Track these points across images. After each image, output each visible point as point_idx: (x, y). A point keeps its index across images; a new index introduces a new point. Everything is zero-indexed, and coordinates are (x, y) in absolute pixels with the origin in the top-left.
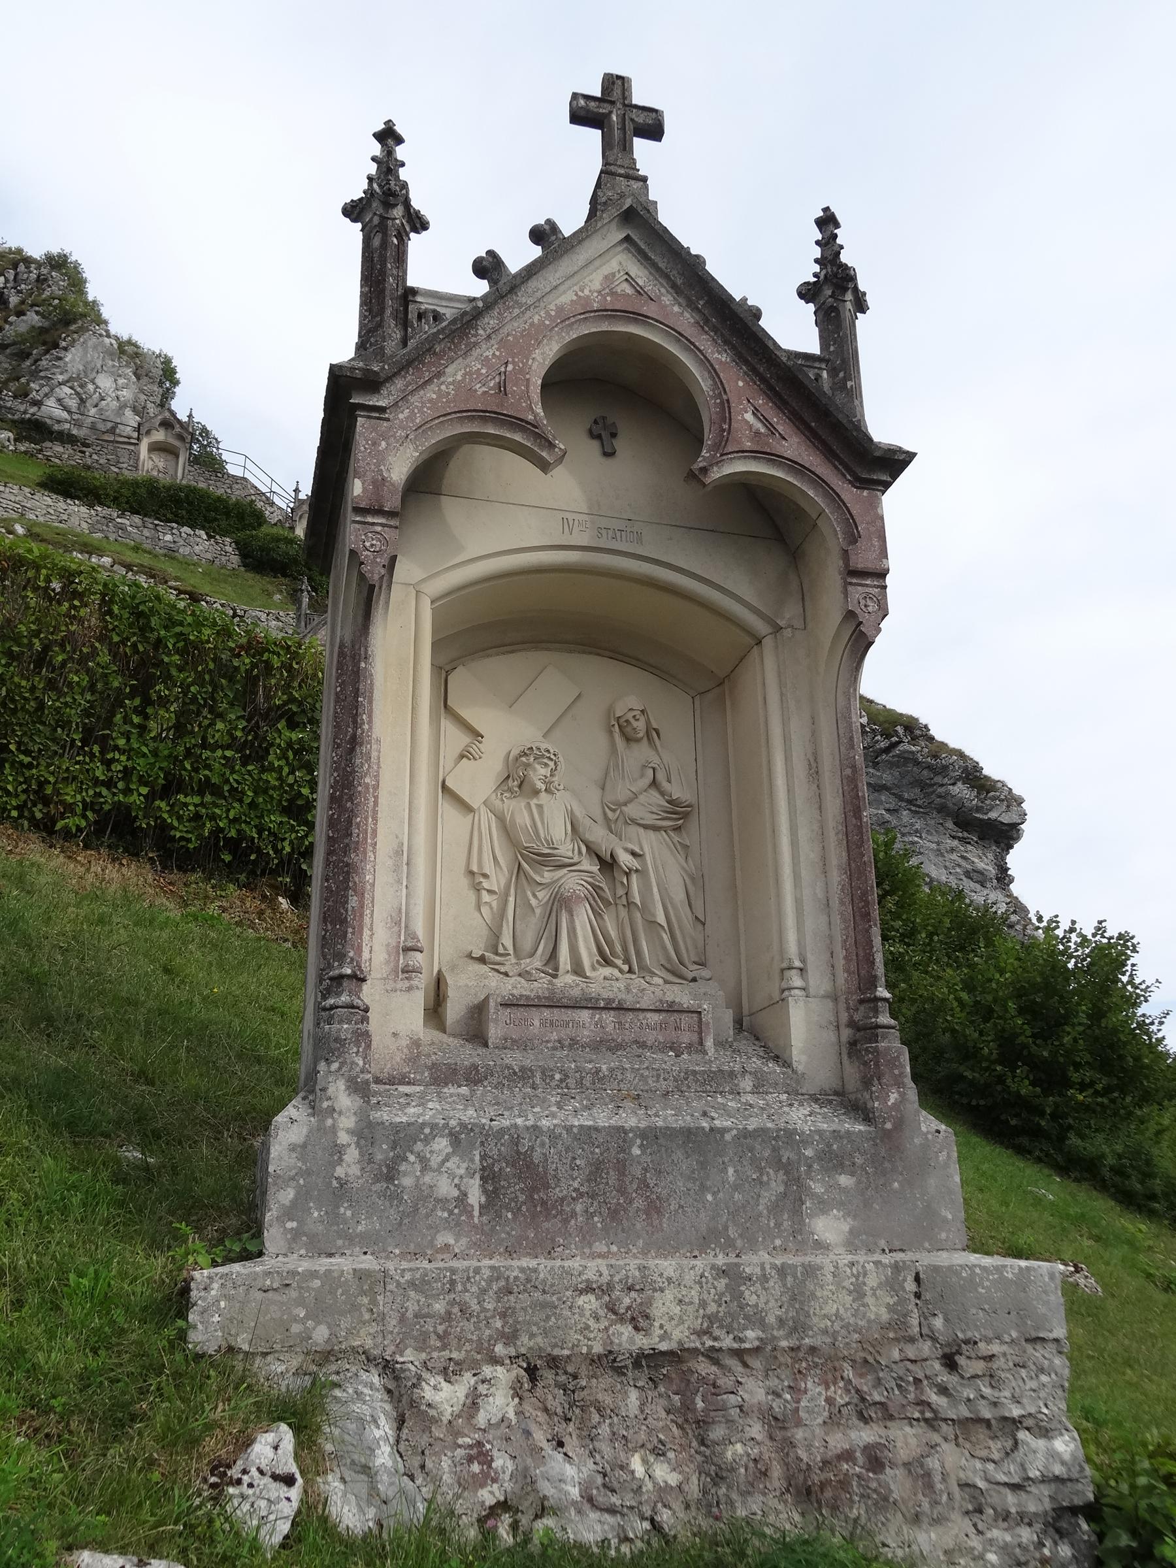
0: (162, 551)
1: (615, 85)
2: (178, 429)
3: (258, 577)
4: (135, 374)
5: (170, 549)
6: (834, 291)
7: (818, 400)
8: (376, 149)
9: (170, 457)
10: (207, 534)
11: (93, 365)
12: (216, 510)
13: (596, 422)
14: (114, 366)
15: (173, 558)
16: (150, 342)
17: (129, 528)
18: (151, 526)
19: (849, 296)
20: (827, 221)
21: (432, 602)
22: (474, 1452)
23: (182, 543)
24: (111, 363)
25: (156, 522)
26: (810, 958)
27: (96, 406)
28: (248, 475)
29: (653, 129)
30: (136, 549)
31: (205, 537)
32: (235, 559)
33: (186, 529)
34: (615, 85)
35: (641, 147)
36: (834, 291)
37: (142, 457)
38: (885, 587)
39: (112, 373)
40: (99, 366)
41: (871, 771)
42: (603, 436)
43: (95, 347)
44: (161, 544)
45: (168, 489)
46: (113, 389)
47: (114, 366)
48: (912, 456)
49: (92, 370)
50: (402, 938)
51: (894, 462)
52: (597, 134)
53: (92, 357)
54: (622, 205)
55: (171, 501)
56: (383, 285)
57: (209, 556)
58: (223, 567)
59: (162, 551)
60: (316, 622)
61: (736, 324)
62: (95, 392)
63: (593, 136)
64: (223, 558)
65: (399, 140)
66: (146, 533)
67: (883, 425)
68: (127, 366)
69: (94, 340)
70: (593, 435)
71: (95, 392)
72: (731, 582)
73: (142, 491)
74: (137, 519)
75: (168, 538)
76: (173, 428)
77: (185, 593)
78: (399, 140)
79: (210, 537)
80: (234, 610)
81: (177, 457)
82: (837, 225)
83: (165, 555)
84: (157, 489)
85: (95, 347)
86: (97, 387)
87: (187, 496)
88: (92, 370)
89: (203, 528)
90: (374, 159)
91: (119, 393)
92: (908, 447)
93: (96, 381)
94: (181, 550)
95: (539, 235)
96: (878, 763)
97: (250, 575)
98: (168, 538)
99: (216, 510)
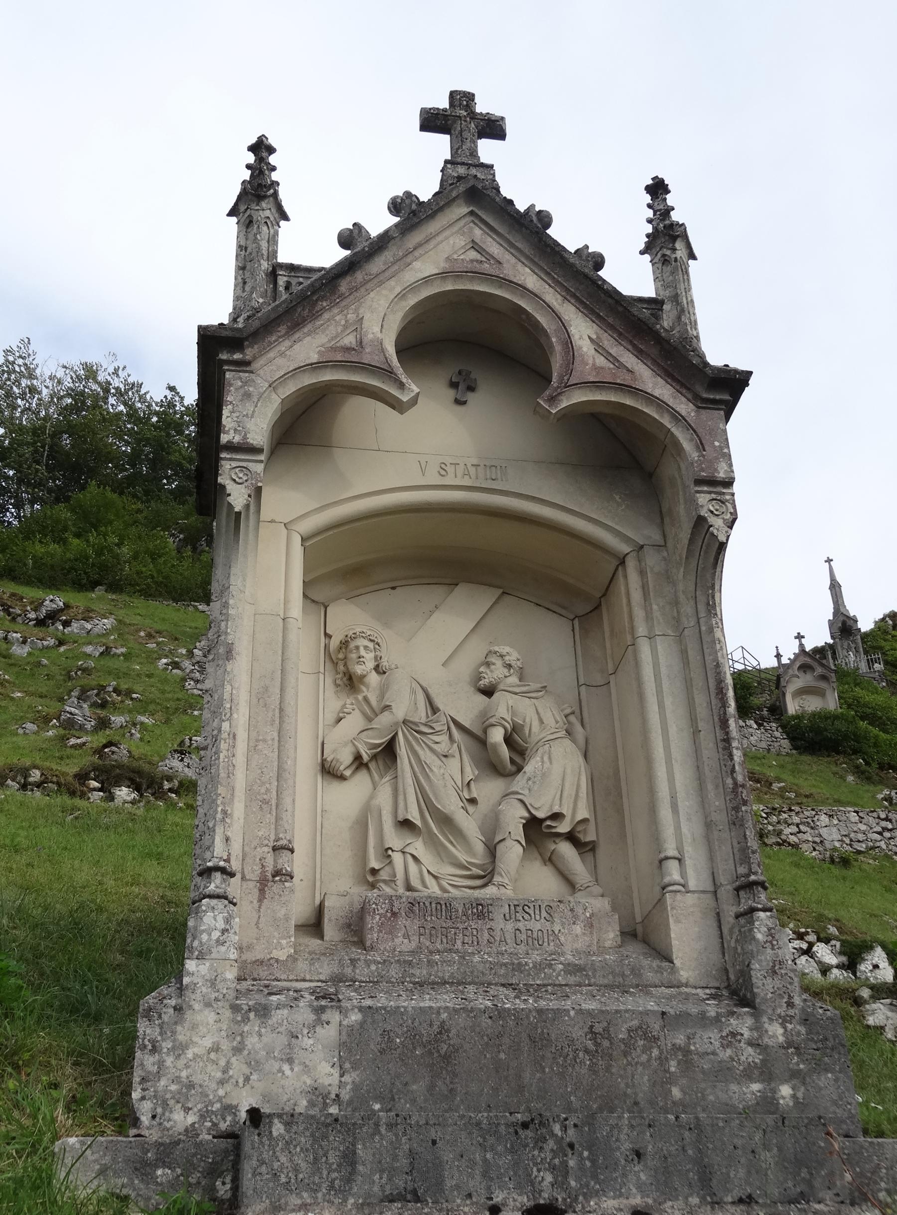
1: (462, 100)
6: (667, 240)
7: (655, 331)
8: (251, 158)
10: (756, 722)
19: (679, 245)
20: (657, 189)
21: (303, 540)
26: (689, 850)
29: (494, 128)
31: (755, 726)
32: (786, 743)
34: (462, 100)
36: (667, 240)
38: (733, 494)
42: (462, 387)
48: (752, 373)
50: (215, 524)
51: (732, 384)
54: (471, 189)
56: (255, 260)
61: (580, 274)
64: (776, 744)
65: (271, 150)
67: (717, 351)
70: (454, 385)
72: (595, 517)
78: (271, 150)
79: (760, 725)
82: (668, 192)
90: (248, 167)
92: (738, 363)
95: (395, 206)
97: (806, 758)
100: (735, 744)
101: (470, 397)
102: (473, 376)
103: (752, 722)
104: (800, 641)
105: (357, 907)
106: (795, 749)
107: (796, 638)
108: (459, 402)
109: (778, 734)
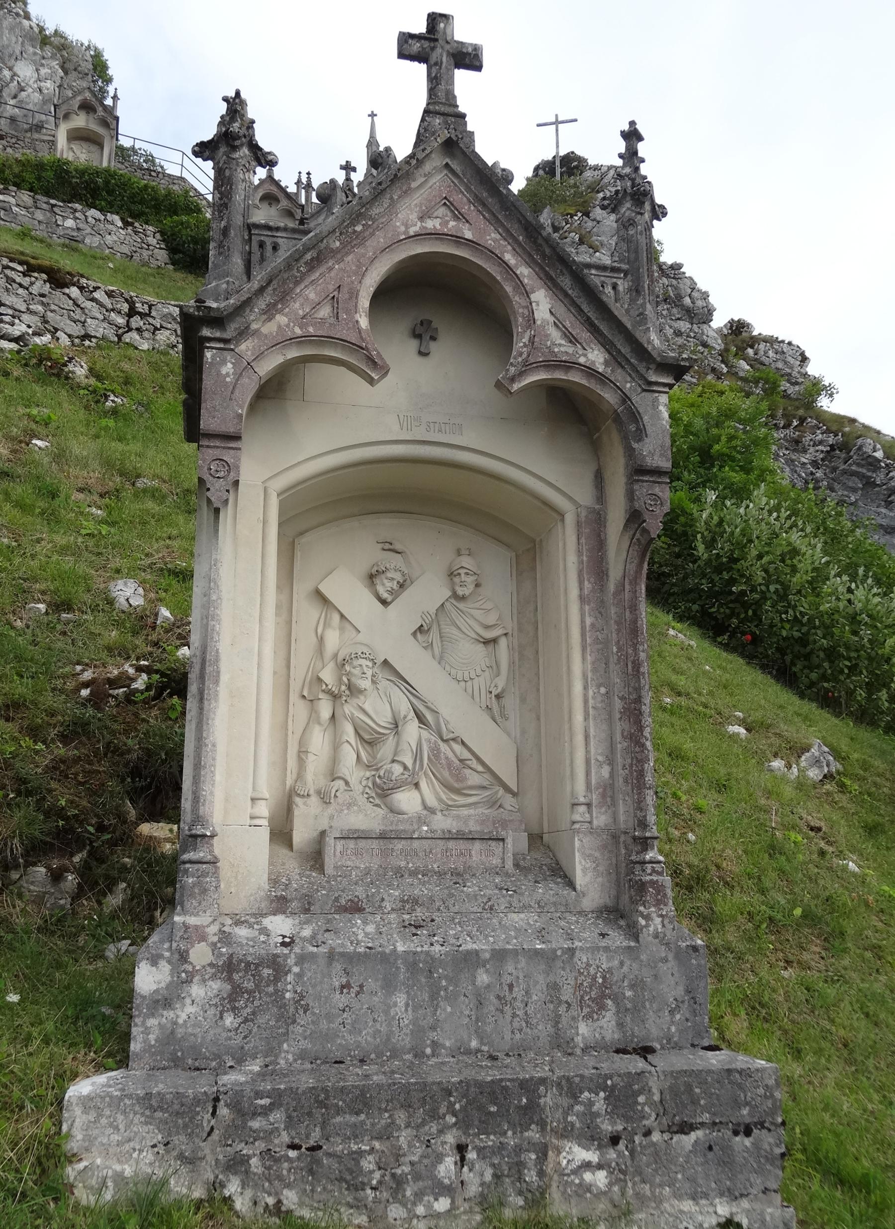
0: (62, 241)
2: (100, 112)
3: (191, 278)
4: (62, 67)
5: (72, 239)
9: (94, 148)
10: (122, 219)
11: (10, 50)
12: (142, 202)
13: (422, 323)
14: (35, 54)
15: (75, 250)
16: (78, 32)
17: (15, 209)
18: (45, 206)
22: (325, 709)
23: (89, 230)
24: (31, 50)
25: (53, 202)
27: (15, 97)
28: (186, 175)
29: (469, 59)
30: (24, 235)
31: (120, 224)
32: (162, 255)
33: (93, 212)
35: (462, 78)
37: (59, 146)
39: (34, 62)
40: (18, 52)
41: (883, 510)
43: (12, 29)
44: (60, 231)
45: (82, 172)
46: (35, 79)
47: (35, 54)
49: (10, 56)
52: (423, 67)
53: (9, 40)
55: (85, 188)
57: (126, 249)
58: (146, 264)
59: (62, 241)
60: (283, 254)
62: (12, 79)
63: (420, 70)
64: (145, 253)
66: (39, 215)
68: (53, 57)
69: (10, 19)
70: (417, 336)
71: (12, 79)
73: (50, 174)
74: (25, 197)
75: (70, 223)
76: (94, 111)
77: (41, 269)
79: (126, 224)
80: (131, 303)
81: (101, 147)
83: (64, 245)
84: (67, 172)
85: (12, 29)
86: (15, 74)
87: (107, 183)
88: (10, 56)
89: (117, 214)
91: (42, 84)
93: (15, 69)
94: (87, 241)
96: (891, 502)
97: (179, 275)
98: (70, 223)
99: (142, 202)
100: (647, 732)
101: (433, 346)
102: (434, 325)
103: (117, 219)
104: (348, 175)
105: (315, 834)
106: (173, 264)
107: (342, 168)
108: (423, 354)
109: (152, 241)
